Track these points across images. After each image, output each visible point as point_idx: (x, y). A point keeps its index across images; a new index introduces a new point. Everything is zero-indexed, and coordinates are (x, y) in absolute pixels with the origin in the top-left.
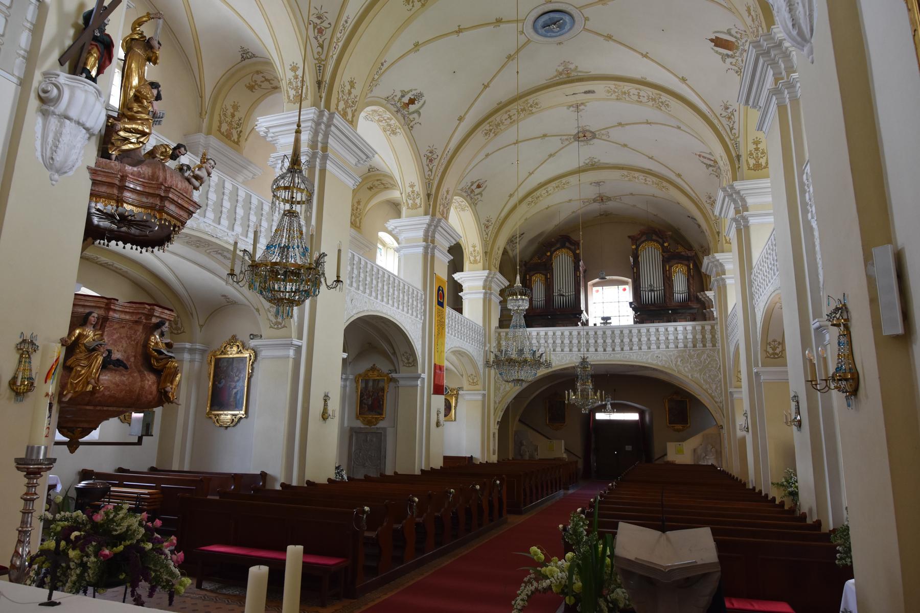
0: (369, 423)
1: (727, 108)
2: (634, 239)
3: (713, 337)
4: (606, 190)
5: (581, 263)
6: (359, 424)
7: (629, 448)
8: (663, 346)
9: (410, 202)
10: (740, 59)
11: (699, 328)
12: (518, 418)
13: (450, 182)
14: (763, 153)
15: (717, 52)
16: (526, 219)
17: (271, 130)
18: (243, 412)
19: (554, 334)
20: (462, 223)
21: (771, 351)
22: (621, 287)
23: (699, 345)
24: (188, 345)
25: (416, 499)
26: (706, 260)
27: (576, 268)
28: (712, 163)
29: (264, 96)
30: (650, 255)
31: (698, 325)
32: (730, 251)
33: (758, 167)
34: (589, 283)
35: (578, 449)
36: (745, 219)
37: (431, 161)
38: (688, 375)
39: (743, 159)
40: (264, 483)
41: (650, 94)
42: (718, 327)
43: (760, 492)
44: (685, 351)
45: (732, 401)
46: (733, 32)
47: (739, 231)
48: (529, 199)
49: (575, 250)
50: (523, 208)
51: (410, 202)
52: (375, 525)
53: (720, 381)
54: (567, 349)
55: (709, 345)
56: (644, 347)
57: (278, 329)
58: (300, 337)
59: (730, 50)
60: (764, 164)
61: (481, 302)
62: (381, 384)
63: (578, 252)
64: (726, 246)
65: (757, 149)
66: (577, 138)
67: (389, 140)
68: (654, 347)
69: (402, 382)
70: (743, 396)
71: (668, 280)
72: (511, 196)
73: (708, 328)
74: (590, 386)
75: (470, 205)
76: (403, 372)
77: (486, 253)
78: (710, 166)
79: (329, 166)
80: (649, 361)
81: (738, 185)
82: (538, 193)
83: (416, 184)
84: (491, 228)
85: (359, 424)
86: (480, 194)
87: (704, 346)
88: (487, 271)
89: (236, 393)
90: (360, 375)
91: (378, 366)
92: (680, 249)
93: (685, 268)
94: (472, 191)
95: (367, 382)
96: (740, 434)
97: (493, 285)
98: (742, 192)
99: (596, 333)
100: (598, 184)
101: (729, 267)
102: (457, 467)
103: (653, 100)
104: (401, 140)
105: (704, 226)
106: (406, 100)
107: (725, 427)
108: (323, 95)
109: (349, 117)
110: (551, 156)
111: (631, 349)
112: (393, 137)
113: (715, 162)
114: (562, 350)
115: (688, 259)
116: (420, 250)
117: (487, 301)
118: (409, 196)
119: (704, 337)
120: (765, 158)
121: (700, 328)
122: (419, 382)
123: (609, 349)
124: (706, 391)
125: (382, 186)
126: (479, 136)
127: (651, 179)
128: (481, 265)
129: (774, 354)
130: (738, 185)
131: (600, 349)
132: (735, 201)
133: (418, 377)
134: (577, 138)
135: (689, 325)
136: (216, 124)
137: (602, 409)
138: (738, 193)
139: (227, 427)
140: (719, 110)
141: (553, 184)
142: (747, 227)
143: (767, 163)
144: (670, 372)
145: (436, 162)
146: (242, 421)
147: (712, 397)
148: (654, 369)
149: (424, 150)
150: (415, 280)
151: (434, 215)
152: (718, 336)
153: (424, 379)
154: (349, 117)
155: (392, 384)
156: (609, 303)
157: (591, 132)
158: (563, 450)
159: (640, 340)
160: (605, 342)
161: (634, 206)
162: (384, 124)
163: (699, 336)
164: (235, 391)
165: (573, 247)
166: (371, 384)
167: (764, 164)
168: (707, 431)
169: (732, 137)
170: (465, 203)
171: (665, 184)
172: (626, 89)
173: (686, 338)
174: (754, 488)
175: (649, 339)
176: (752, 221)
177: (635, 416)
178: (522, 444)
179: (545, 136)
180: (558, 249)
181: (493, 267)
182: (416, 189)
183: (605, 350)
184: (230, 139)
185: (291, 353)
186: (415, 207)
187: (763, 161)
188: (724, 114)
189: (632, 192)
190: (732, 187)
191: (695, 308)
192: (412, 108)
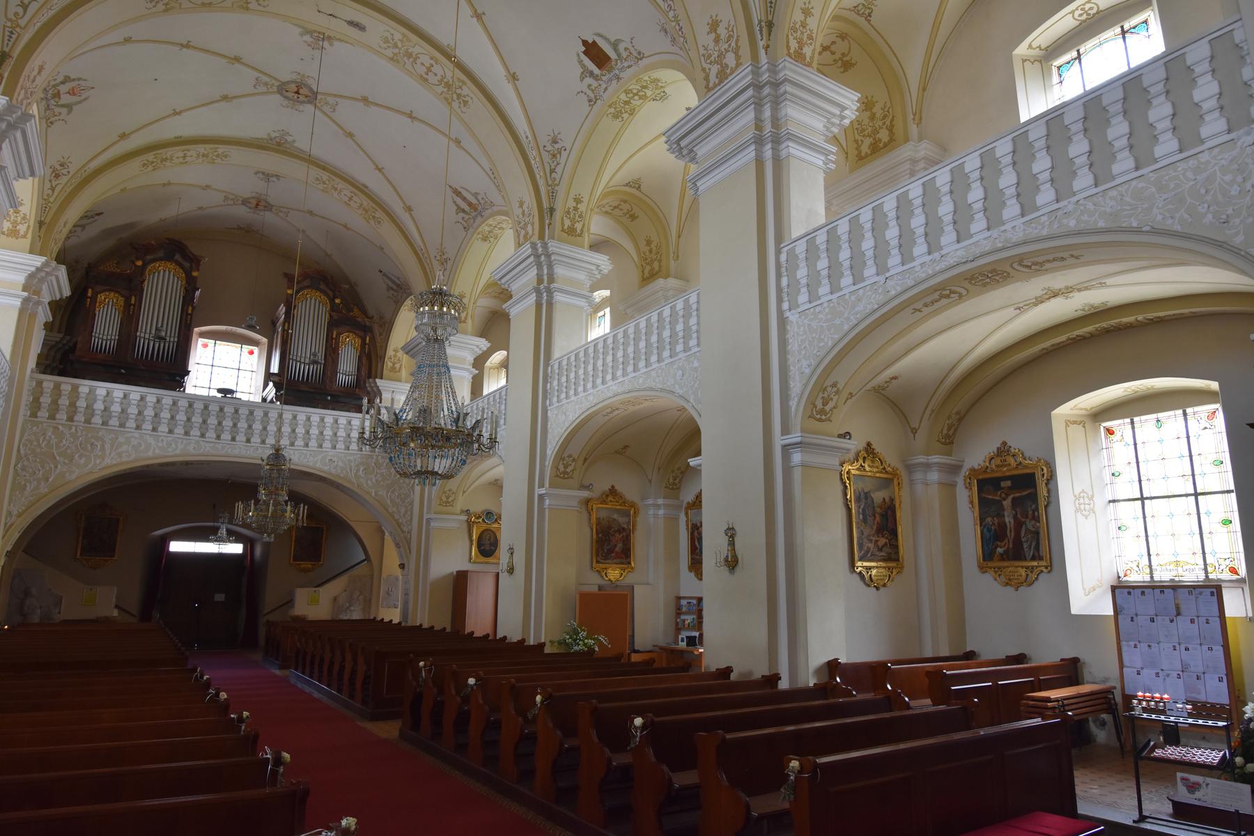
8: (341, 446)
10: (604, 86)
15: (581, 62)
16: (123, 190)
19: (158, 401)
21: (562, 469)
22: (246, 348)
28: (467, 208)
30: (312, 313)
33: (571, 231)
34: (196, 330)
36: (550, 292)
39: (558, 215)
41: (449, 74)
44: (371, 457)
46: (621, 47)
48: (150, 156)
53: (412, 503)
54: (179, 430)
59: (600, 68)
61: (14, 316)
63: (195, 274)
65: (576, 209)
68: (327, 445)
71: (332, 352)
72: (123, 136)
77: (41, 224)
78: (464, 211)
80: (318, 465)
82: (169, 152)
84: (64, 180)
86: (69, 107)
97: (45, 287)
99: (236, 411)
100: (267, 176)
103: (448, 86)
110: (225, 98)
114: (171, 431)
128: (27, 242)
129: (565, 473)
131: (241, 438)
140: (544, 140)
141: (202, 148)
142: (550, 304)
144: (345, 484)
156: (226, 367)
159: (308, 432)
160: (250, 427)
165: (187, 265)
172: (417, 50)
175: (321, 433)
177: (236, 548)
178: (27, 593)
179: (237, 59)
180: (161, 259)
183: (248, 441)
187: (578, 226)
189: (312, 209)
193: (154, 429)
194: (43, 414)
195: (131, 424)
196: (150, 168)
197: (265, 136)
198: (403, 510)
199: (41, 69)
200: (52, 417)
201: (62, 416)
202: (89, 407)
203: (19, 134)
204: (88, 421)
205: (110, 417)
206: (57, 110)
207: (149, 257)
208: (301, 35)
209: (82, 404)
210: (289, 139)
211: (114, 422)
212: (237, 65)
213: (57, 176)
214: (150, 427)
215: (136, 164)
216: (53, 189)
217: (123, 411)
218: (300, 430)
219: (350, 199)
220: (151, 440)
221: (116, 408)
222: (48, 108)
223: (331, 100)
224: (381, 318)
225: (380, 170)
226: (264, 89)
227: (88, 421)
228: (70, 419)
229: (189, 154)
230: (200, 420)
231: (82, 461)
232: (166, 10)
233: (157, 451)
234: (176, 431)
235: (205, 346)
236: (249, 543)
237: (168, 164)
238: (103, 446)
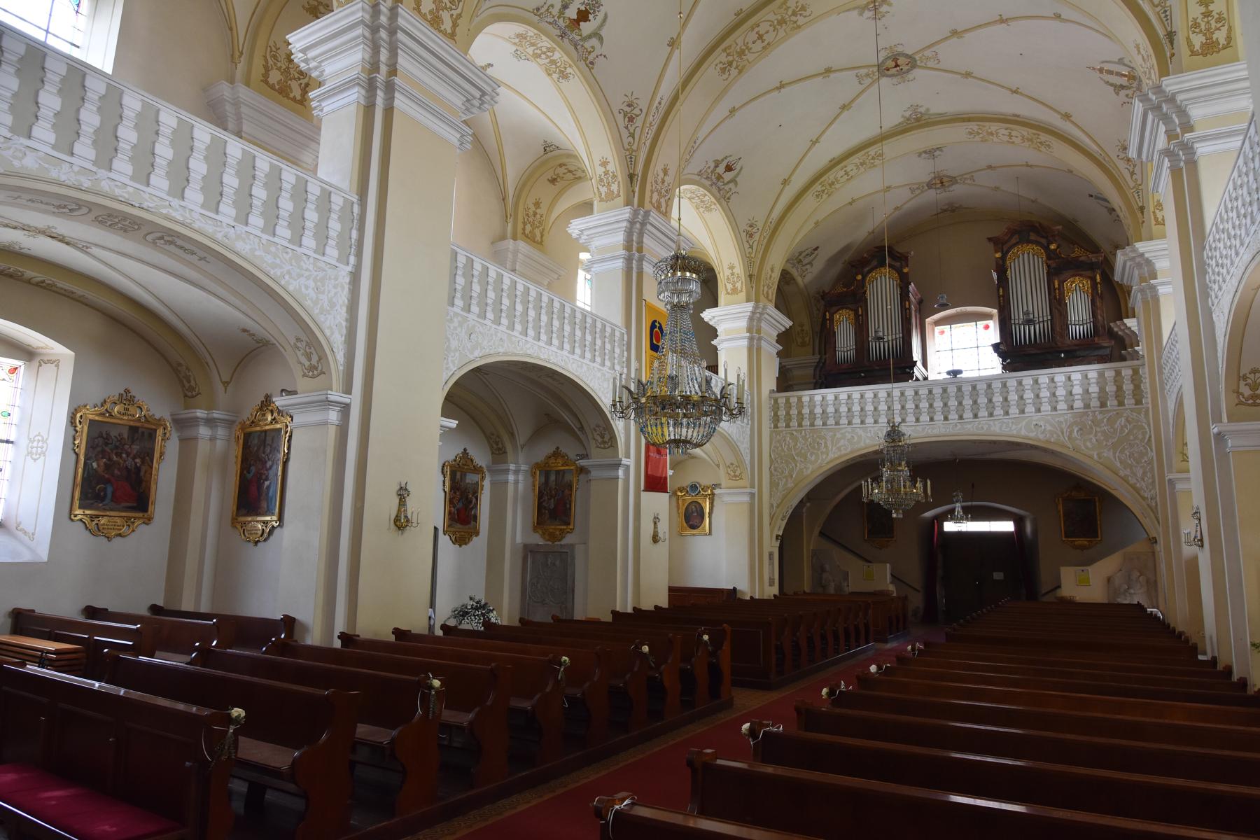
0: (553, 537)
2: (998, 243)
4: (947, 164)
5: (912, 287)
6: (537, 539)
7: (998, 576)
8: (1046, 407)
9: (603, 190)
11: (1110, 374)
12: (817, 531)
13: (667, 155)
14: (1219, 20)
16: (817, 223)
17: (311, 54)
18: (275, 518)
20: (700, 223)
21: (1247, 391)
22: (981, 324)
23: (1111, 403)
24: (200, 413)
25: (436, 683)
26: (1120, 257)
27: (904, 295)
28: (1124, 81)
29: (569, 186)
30: (1027, 267)
31: (1109, 369)
32: (1164, 236)
35: (915, 574)
36: (1189, 148)
37: (631, 119)
38: (1095, 457)
39: (1180, 39)
40: (290, 634)
42: (1145, 372)
43: (1228, 671)
45: (1173, 495)
47: (1176, 173)
48: (818, 187)
49: (902, 267)
50: (809, 201)
51: (603, 190)
52: (554, 692)
53: (1150, 462)
55: (1129, 401)
57: (313, 377)
58: (348, 390)
60: (1222, 41)
62: (568, 477)
63: (905, 270)
64: (1155, 229)
66: (882, 70)
67: (560, 90)
68: (1030, 409)
69: (594, 474)
70: (1192, 490)
71: (1058, 305)
72: (785, 182)
73: (1126, 373)
74: (905, 471)
75: (718, 200)
76: (597, 457)
77: (751, 276)
78: (1122, 87)
79: (400, 102)
80: (1023, 433)
81: (1171, 84)
82: (831, 176)
83: (610, 159)
84: (756, 237)
85: (537, 539)
86: (733, 181)
87: (1121, 404)
88: (752, 304)
89: (268, 487)
90: (537, 466)
91: (563, 450)
92: (1078, 252)
93: (1087, 284)
94: (719, 177)
95: (547, 474)
96: (1188, 550)
97: (763, 325)
98: (1180, 98)
99: (930, 392)
100: (931, 153)
101: (1161, 265)
102: (694, 607)
104: (577, 86)
105: (1116, 200)
106: (572, 13)
107: (1161, 540)
108: (637, 189)
109: (447, 25)
110: (844, 107)
111: (991, 415)
112: (564, 83)
113: (1132, 77)
114: (876, 422)
115: (1092, 267)
117: (754, 350)
118: (601, 180)
119: (1119, 389)
120: (1224, 29)
121: (1113, 373)
122: (621, 472)
123: (953, 416)
124: (1125, 479)
125: (569, 176)
126: (710, 72)
127: (1019, 131)
128: (743, 295)
130: (1171, 84)
131: (939, 417)
132: (1166, 118)
133: (618, 465)
134: (882, 70)
135: (1092, 370)
136: (258, 70)
137: (950, 515)
138: (1171, 99)
139: (256, 543)
141: (855, 159)
142: (1193, 164)
143: (1229, 38)
145: (639, 122)
146: (276, 532)
147: (1137, 491)
148: (1032, 447)
149: (618, 103)
150: (615, 316)
151: (641, 204)
152: (1146, 386)
153: (628, 467)
154: (447, 25)
155: (582, 477)
157: (907, 56)
158: (889, 576)
159: (1006, 399)
160: (945, 405)
161: (997, 188)
162: (543, 60)
163: (1111, 388)
164: (267, 483)
165: (898, 264)
166: (553, 478)
167: (1222, 41)
168: (1129, 549)
170: (709, 198)
171: (1044, 137)
173: (1087, 392)
174: (1214, 661)
175: (1021, 398)
176: (1202, 149)
177: (1007, 526)
178: (823, 570)
181: (762, 297)
182: (611, 168)
183: (946, 419)
184: (287, 96)
185: (333, 416)
186: (610, 196)
187: (1220, 36)
189: (993, 164)
190: (1158, 89)
191: (1108, 343)
192: (587, 28)
193: (862, 422)
194: (782, 424)
195: (844, 421)
196: (825, 196)
197: (901, 120)
198: (1140, 472)
199: (665, 172)
200: (788, 426)
201: (794, 423)
203: (649, 227)
206: (727, 188)
207: (866, 269)
208: (861, 14)
209: (806, 411)
210: (922, 110)
211: (831, 421)
212: (832, 75)
213: (751, 236)
215: (809, 199)
216: (751, 247)
217: (836, 411)
219: (1010, 136)
220: (861, 432)
221: (831, 409)
222: (719, 190)
223: (928, 53)
225: (1015, 92)
226: (870, 80)
227: (812, 425)
228: (800, 425)
229: (848, 169)
232: (740, 72)
235: (942, 332)
236: (1019, 522)
237: (837, 186)
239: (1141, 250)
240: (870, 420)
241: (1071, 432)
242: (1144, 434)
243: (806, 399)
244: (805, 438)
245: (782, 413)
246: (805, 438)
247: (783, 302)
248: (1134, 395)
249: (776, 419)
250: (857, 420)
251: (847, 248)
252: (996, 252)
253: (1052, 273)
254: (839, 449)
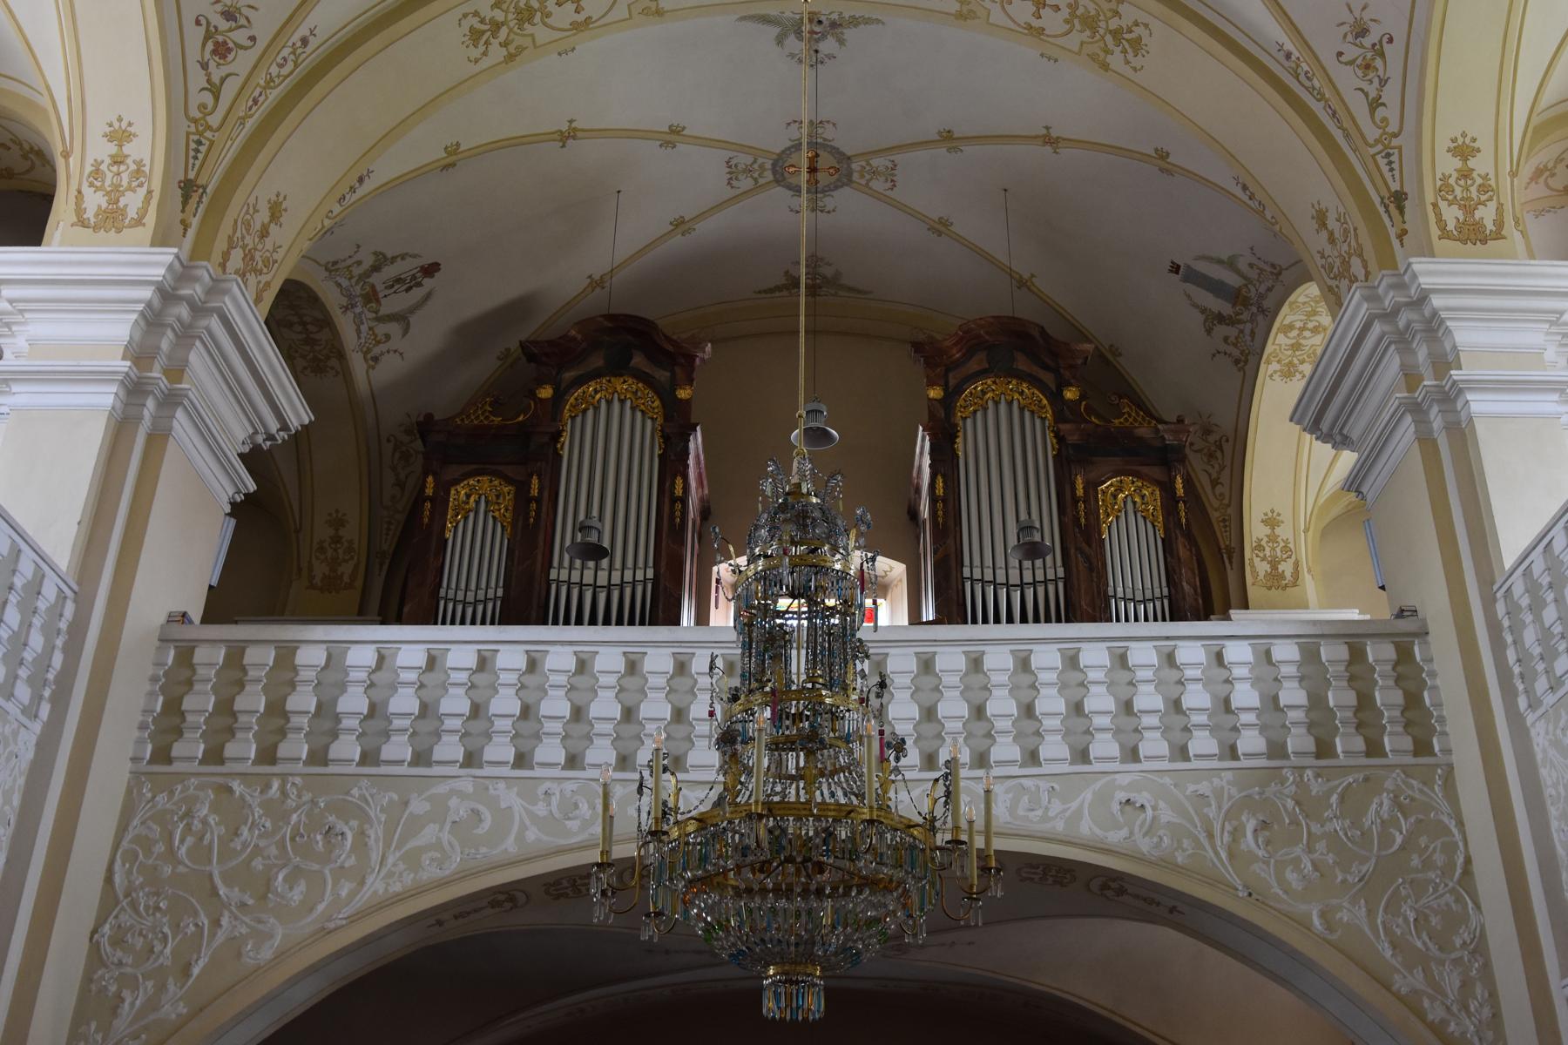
1: (1362, 32)
3: (1413, 701)
5: (696, 442)
8: (1154, 745)
23: (1346, 743)
46: (394, 328)
49: (675, 385)
53: (1479, 947)
55: (1395, 742)
56: (1054, 748)
63: (683, 394)
68: (1105, 746)
77: (188, 188)
79: (181, 422)
80: (1086, 828)
84: (242, 63)
88: (167, 255)
93: (1152, 494)
97: (197, 359)
114: (573, 761)
116: (105, 397)
119: (1365, 701)
124: (1411, 1003)
159: (1028, 711)
161: (941, 227)
163: (1339, 697)
165: (662, 375)
169: (1372, 133)
173: (1272, 703)
175: (1077, 708)
188: (1351, 52)
193: (522, 760)
194: (191, 747)
195: (450, 749)
198: (1451, 981)
199: (276, 211)
200: (215, 756)
201: (244, 748)
202: (326, 711)
204: (319, 757)
205: (386, 734)
207: (569, 375)
209: (303, 701)
211: (398, 748)
213: (222, 51)
214: (509, 754)
216: (215, 90)
218: (1002, 705)
220: (509, 798)
224: (1207, 431)
227: (319, 757)
228: (268, 755)
230: (666, 712)
231: (297, 895)
233: (532, 835)
234: (591, 756)
238: (361, 834)
239: (1425, 281)
240: (551, 751)
241: (1237, 833)
242: (1450, 849)
243: (311, 657)
244: (277, 811)
245: (199, 702)
246: (277, 811)
247: (297, 319)
248: (1408, 725)
249: (168, 724)
250: (500, 750)
251: (519, 308)
252: (931, 384)
253: (1068, 459)
254: (413, 860)
